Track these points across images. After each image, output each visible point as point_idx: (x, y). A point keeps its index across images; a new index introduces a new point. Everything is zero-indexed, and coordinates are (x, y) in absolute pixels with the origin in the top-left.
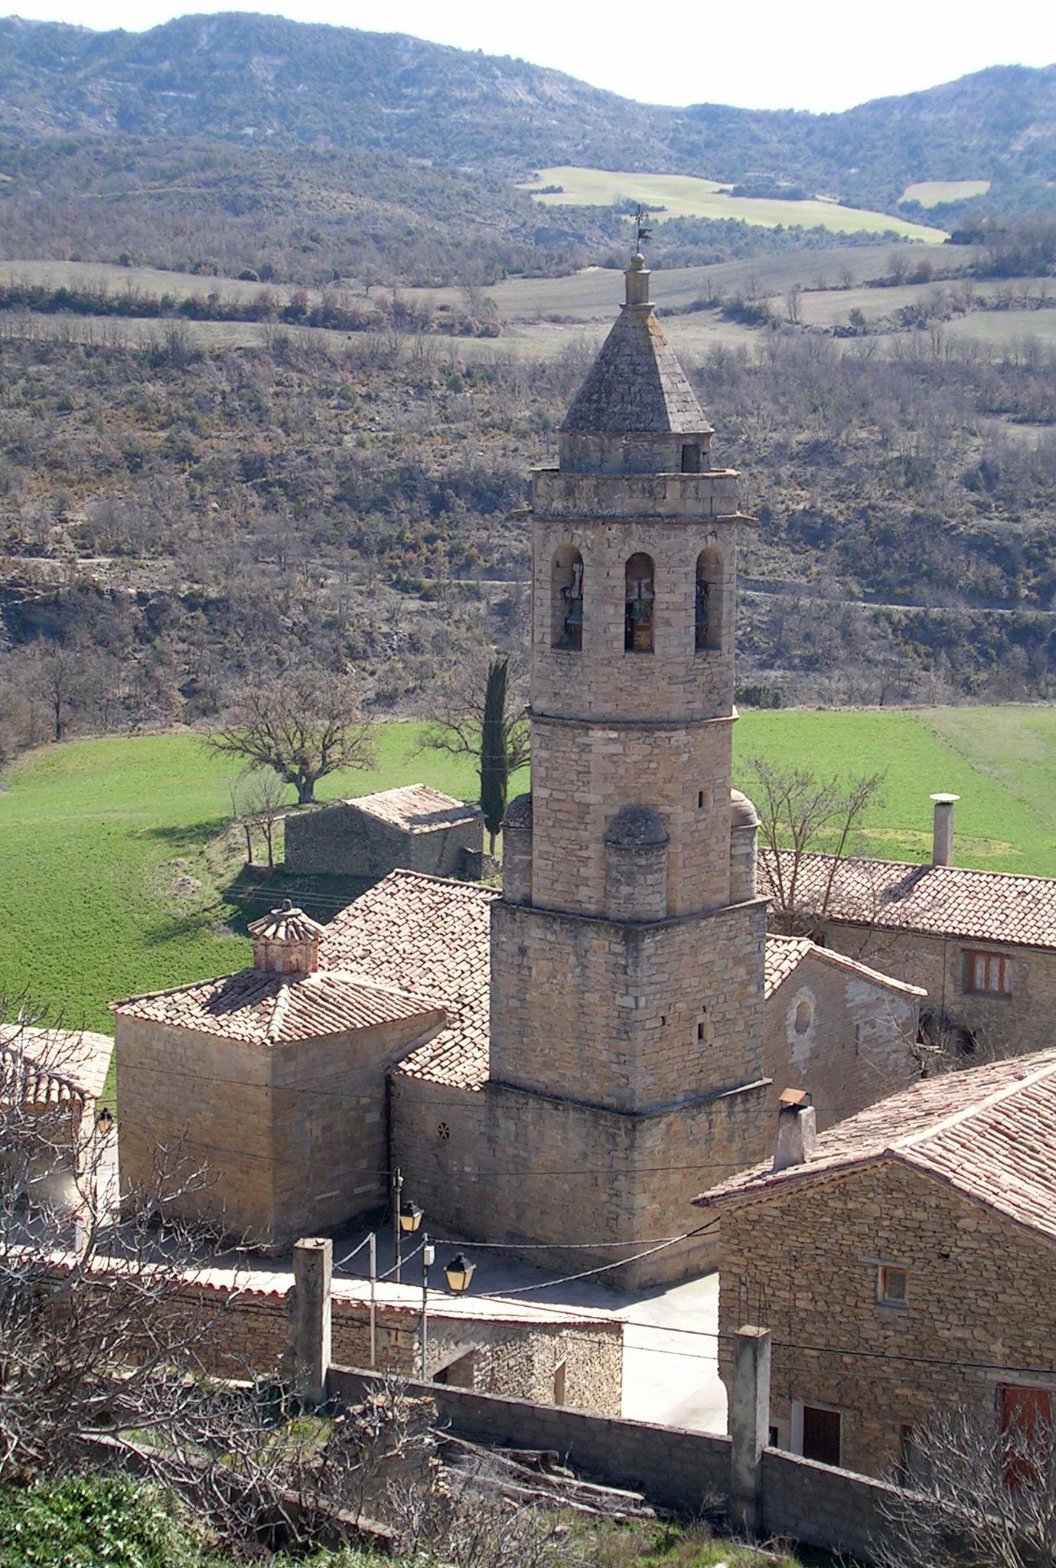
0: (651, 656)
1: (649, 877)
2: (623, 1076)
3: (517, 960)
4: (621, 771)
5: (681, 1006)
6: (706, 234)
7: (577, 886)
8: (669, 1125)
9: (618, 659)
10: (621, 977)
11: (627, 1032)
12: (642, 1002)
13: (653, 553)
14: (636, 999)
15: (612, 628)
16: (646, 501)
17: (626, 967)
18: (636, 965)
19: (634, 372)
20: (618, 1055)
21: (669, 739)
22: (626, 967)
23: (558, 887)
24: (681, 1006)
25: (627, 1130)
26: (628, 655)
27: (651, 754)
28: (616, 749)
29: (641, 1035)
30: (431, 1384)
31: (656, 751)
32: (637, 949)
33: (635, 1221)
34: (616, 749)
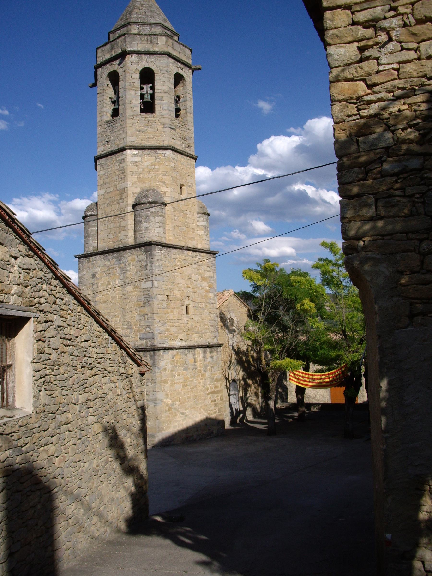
0: (154, 114)
1: (156, 218)
2: (147, 327)
3: (92, 281)
4: (140, 170)
5: (176, 292)
6: (167, 444)
7: (120, 232)
8: (173, 357)
9: (137, 116)
10: (144, 272)
11: (148, 302)
12: (156, 283)
13: (153, 67)
14: (153, 282)
15: (134, 101)
16: (149, 45)
17: (146, 266)
18: (151, 263)
19: (142, 6)
20: (144, 315)
21: (164, 154)
22: (146, 266)
23: (111, 236)
24: (176, 292)
25: (151, 356)
26: (142, 114)
27: (155, 161)
28: (138, 159)
29: (156, 303)
30: (234, 409)
31: (158, 160)
32: (151, 255)
33: (158, 407)
34: (138, 159)
